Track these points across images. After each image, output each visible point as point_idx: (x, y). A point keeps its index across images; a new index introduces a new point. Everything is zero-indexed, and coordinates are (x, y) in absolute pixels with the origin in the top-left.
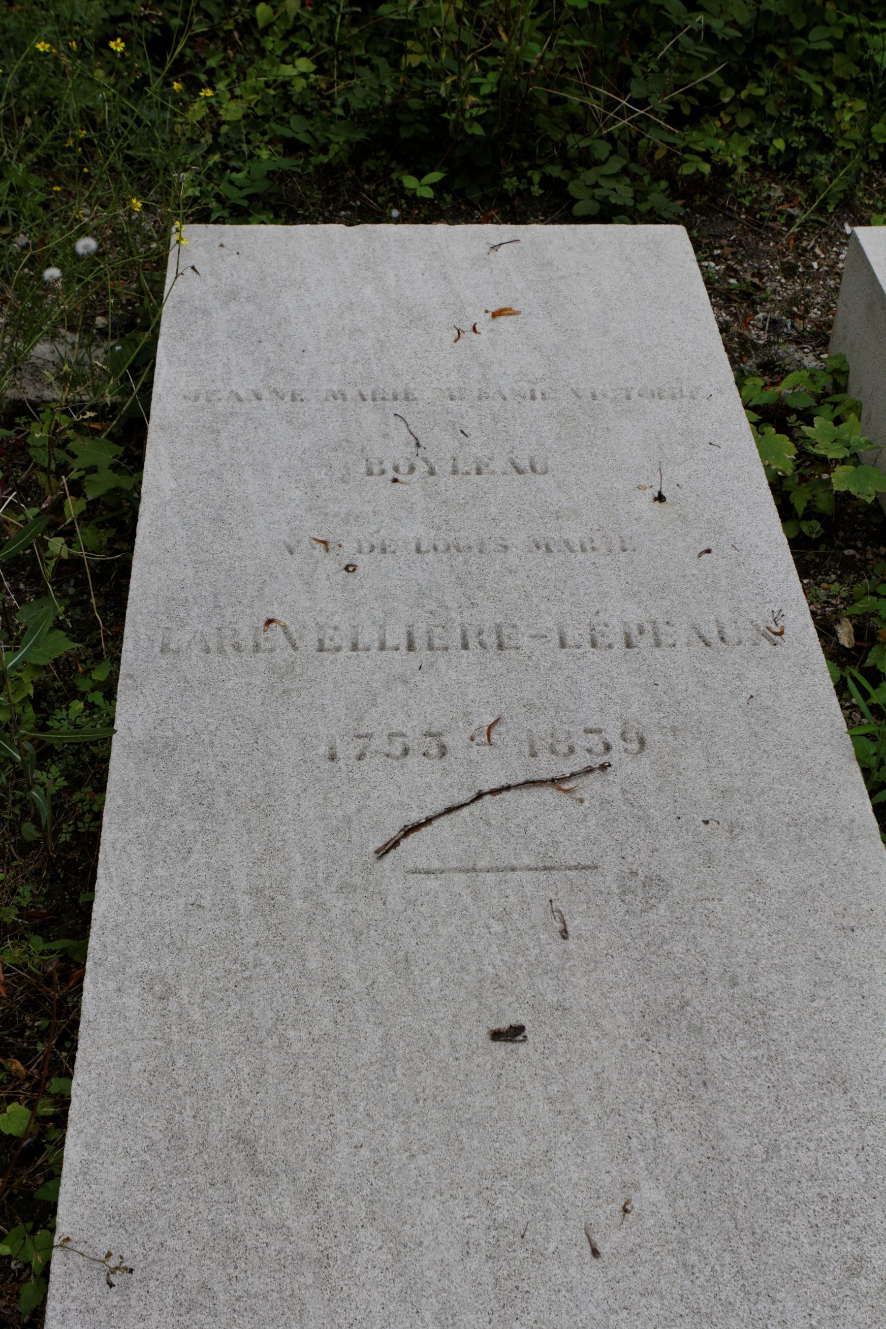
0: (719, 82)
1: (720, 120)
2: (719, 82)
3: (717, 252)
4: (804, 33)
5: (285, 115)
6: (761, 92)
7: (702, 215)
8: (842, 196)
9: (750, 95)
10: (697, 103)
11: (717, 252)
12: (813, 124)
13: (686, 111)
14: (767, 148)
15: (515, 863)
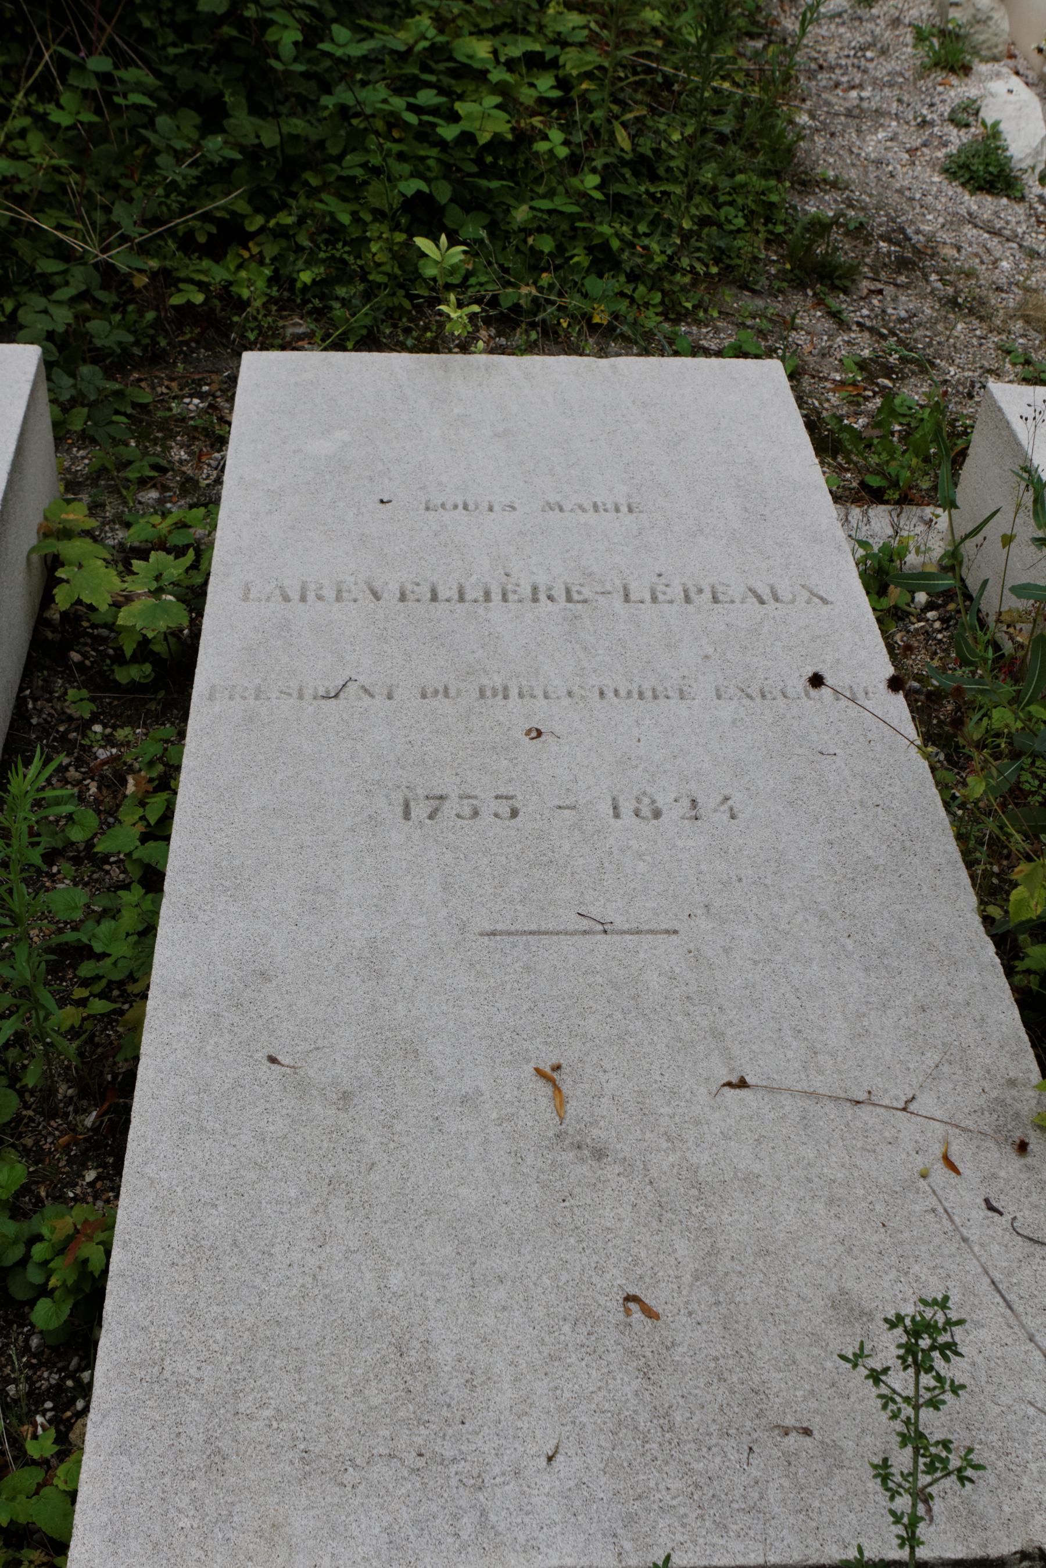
0: (242, 207)
1: (248, 249)
2: (242, 207)
3: (205, 388)
4: (339, 159)
5: (125, 183)
6: (289, 220)
7: (207, 350)
8: (364, 332)
9: (278, 224)
10: (214, 231)
11: (205, 388)
12: (338, 255)
13: (202, 239)
14: (295, 280)
15: (807, 1103)
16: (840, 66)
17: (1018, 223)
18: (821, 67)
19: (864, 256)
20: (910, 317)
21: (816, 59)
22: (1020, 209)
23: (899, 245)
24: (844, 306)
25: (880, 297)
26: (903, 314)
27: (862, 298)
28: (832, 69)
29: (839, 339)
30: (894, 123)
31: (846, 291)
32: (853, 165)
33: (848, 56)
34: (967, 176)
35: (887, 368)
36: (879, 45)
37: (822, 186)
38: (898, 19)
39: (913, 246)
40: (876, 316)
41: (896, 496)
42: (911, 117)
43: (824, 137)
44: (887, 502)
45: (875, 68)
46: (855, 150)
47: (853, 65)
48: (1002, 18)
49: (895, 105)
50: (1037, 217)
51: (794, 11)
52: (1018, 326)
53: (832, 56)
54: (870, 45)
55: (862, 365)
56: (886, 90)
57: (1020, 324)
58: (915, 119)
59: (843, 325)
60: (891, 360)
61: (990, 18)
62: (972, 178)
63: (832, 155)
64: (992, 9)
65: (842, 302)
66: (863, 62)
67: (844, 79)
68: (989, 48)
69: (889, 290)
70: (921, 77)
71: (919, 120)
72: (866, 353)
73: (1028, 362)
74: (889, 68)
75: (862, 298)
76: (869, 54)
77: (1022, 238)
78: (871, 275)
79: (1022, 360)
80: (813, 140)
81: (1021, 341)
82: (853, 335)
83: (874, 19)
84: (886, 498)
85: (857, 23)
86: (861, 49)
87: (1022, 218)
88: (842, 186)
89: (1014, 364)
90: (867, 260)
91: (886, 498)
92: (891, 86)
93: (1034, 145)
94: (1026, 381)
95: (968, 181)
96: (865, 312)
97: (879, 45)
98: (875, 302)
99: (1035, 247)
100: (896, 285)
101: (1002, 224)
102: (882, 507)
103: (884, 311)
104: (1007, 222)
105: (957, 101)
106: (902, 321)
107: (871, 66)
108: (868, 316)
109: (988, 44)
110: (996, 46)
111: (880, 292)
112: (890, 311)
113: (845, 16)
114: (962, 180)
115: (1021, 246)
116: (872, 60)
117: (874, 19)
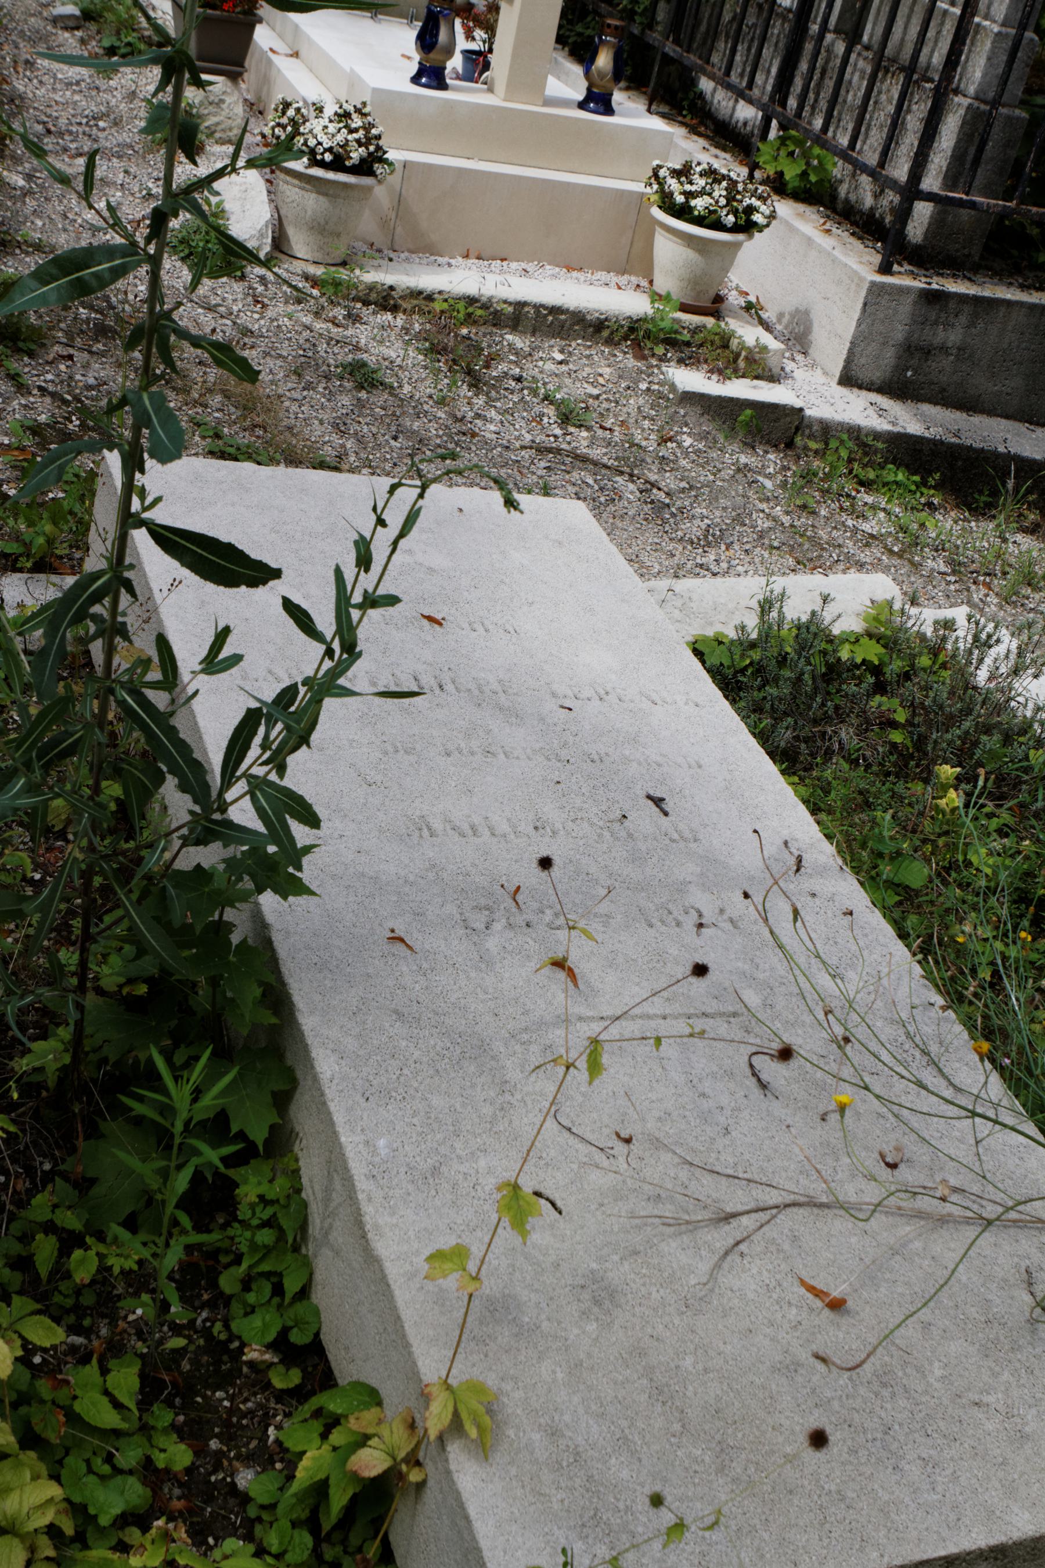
16: (70, 133)
17: (235, 300)
18: (49, 132)
19: (60, 321)
20: (100, 385)
21: (44, 123)
22: (238, 287)
23: (102, 313)
24: (26, 370)
25: (69, 363)
26: (91, 381)
27: (47, 362)
28: (61, 134)
29: (16, 402)
30: (119, 194)
31: (31, 355)
32: (65, 230)
33: (80, 124)
34: (187, 251)
35: (65, 434)
36: (112, 117)
37: (24, 247)
38: (134, 92)
39: (117, 315)
40: (62, 382)
41: (29, 565)
42: (136, 189)
43: (38, 200)
44: (21, 570)
45: (106, 138)
46: (71, 216)
47: (84, 133)
48: (236, 103)
49: (121, 175)
50: (254, 296)
51: (28, 73)
52: (217, 400)
53: (62, 121)
54: (103, 115)
55: (35, 430)
56: (115, 160)
57: (218, 398)
58: (140, 191)
59: (22, 389)
60: (71, 426)
61: (222, 101)
62: (191, 254)
63: (41, 218)
64: (224, 93)
65: (26, 365)
66: (95, 131)
67: (73, 146)
68: (223, 130)
69: (80, 357)
70: (151, 151)
71: (144, 192)
72: (43, 418)
73: (217, 436)
74: (120, 140)
75: (47, 362)
76: (101, 124)
77: (237, 316)
78: (64, 340)
79: (211, 433)
80: (24, 203)
81: (216, 415)
82: (32, 399)
83: (110, 90)
84: (19, 565)
85: (94, 93)
86: (94, 118)
87: (240, 296)
88: (47, 249)
89: (203, 438)
90: (62, 325)
91: (19, 565)
92: (119, 157)
93: (259, 227)
94: (212, 454)
95: (188, 256)
96: (49, 377)
97: (112, 117)
98: (62, 367)
99: (250, 326)
100: (90, 352)
101: (218, 300)
102: (19, 575)
103: (71, 378)
104: (224, 299)
105: (184, 177)
106: (90, 388)
107: (101, 135)
108: (53, 381)
109: (223, 126)
110: (230, 129)
111: (70, 357)
112: (78, 377)
113: (83, 85)
114: (182, 255)
115: (234, 323)
116: (104, 129)
117: (110, 90)
